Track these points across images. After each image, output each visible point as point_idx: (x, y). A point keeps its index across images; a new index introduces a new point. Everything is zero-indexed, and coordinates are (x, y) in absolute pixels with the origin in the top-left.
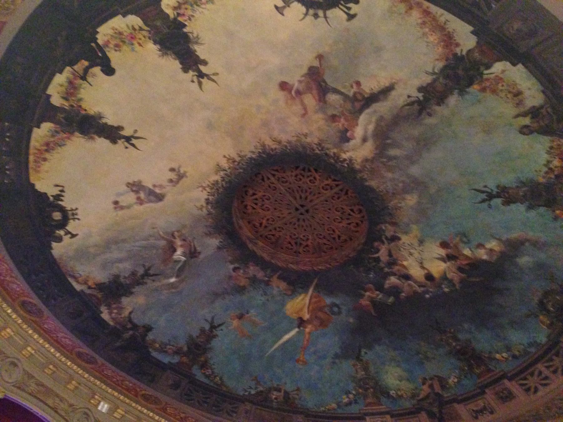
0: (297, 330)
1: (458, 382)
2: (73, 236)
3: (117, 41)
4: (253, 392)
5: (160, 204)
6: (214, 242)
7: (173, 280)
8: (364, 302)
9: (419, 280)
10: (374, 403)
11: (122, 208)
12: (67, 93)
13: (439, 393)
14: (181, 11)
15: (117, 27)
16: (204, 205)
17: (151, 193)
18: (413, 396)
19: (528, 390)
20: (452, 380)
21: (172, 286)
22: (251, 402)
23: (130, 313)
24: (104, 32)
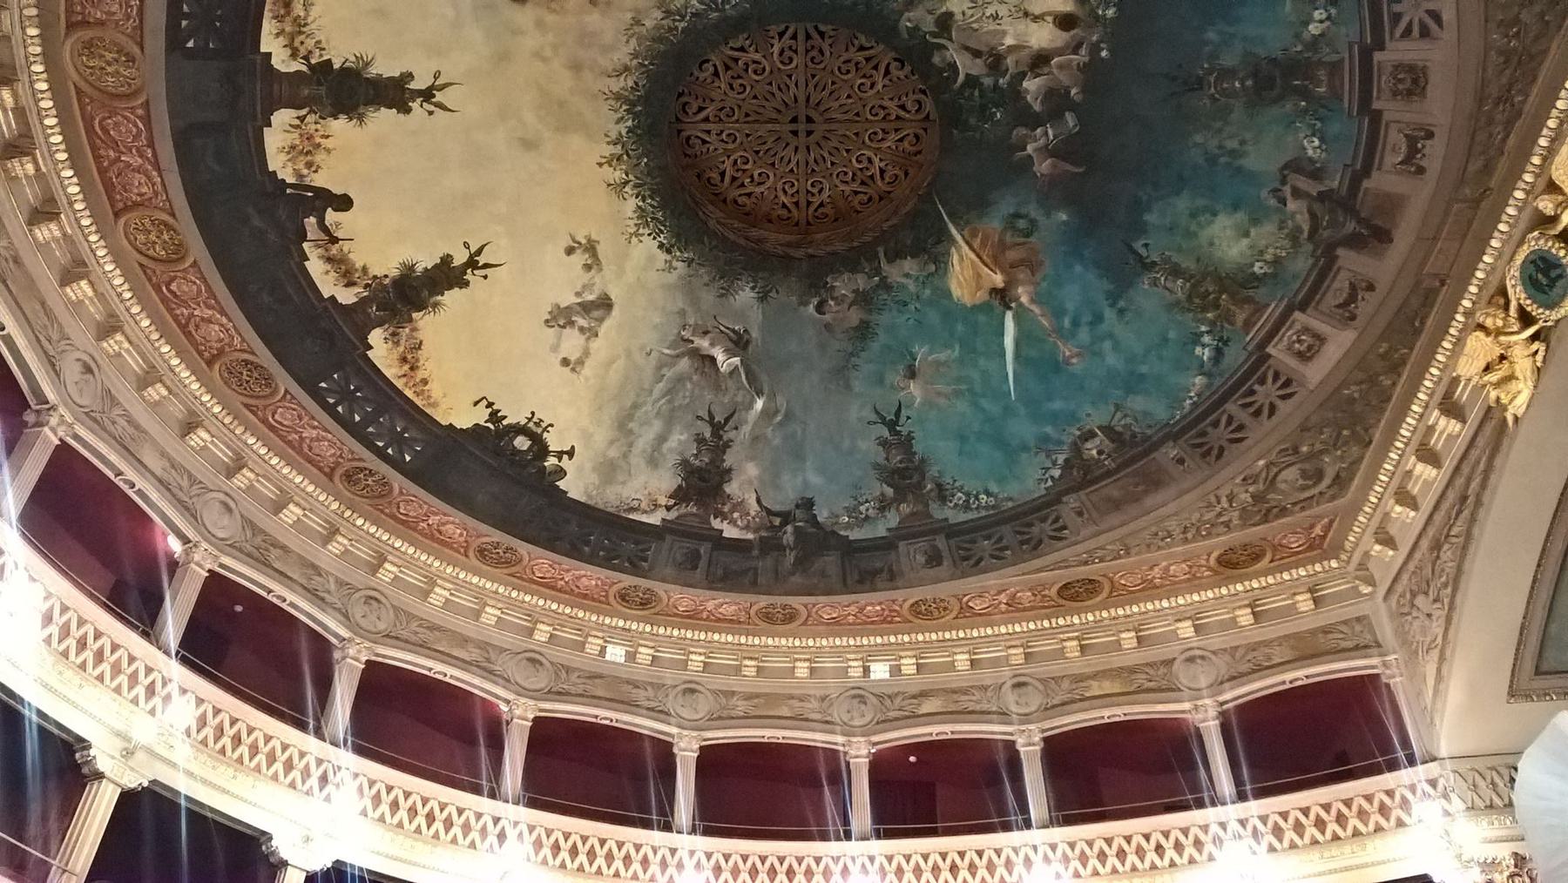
0: (1009, 316)
1: (1322, 140)
2: (571, 454)
3: (302, 160)
4: (1057, 473)
5: (615, 312)
6: (745, 296)
7: (759, 404)
8: (1043, 167)
9: (1059, 43)
10: (1252, 315)
11: (580, 362)
12: (344, 276)
13: (1320, 193)
14: (303, 52)
15: (280, 145)
16: (668, 257)
17: (586, 308)
18: (1294, 238)
19: (1425, 33)
20: (1312, 147)
21: (767, 414)
22: (1067, 492)
23: (759, 501)
24: (279, 163)
